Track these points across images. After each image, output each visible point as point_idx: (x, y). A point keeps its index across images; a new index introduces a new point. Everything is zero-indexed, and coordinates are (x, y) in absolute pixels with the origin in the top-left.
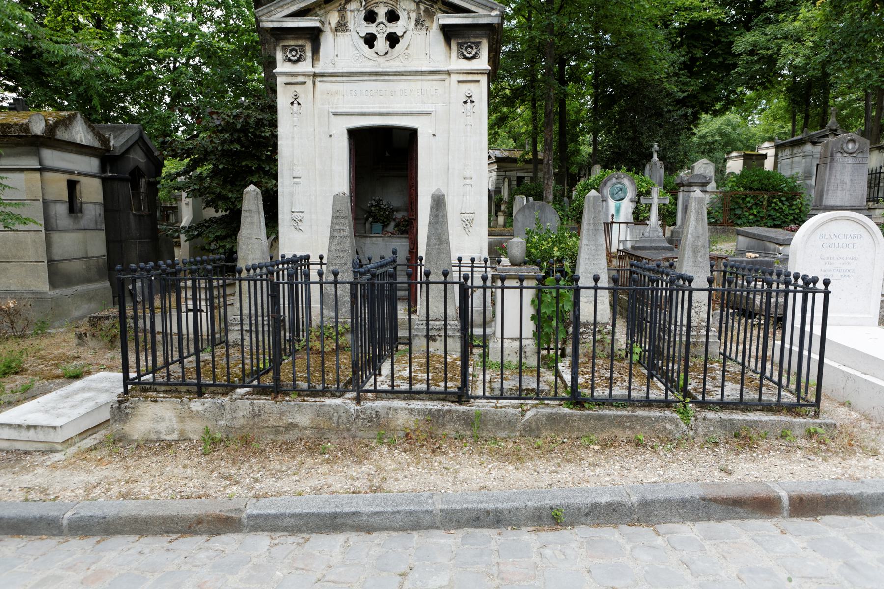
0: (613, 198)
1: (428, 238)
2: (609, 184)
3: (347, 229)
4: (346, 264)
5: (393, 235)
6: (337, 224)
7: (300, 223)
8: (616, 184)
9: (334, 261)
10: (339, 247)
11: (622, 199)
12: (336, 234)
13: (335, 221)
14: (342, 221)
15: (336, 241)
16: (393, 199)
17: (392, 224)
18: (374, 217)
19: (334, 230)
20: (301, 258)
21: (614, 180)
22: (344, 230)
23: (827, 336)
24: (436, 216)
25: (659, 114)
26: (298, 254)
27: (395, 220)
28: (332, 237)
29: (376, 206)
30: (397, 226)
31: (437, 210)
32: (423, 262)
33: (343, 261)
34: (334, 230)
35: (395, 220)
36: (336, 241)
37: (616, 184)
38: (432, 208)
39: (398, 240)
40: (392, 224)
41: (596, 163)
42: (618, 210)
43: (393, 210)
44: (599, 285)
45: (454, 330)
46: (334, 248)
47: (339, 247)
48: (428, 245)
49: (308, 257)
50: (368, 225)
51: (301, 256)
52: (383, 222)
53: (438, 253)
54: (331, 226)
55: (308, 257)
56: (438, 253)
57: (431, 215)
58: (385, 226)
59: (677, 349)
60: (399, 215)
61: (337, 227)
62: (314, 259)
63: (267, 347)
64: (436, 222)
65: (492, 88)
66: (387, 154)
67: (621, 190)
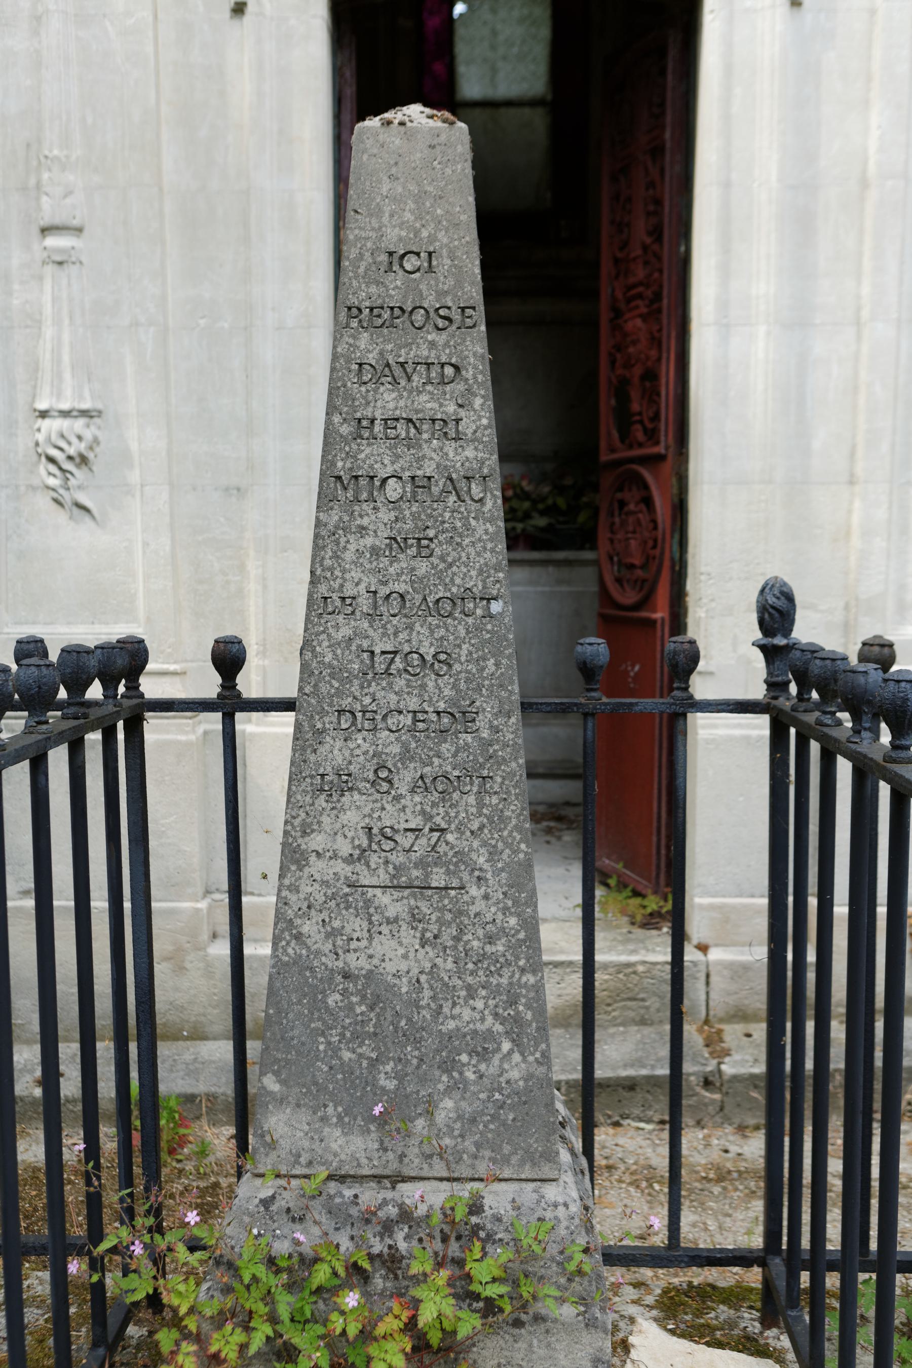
3: (480, 417)
4: (465, 717)
6: (390, 372)
7: (80, 475)
9: (358, 696)
10: (401, 573)
12: (376, 457)
13: (368, 347)
14: (429, 345)
15: (378, 521)
19: (363, 427)
20: (78, 666)
22: (446, 428)
23: (577, 930)
26: (58, 636)
28: (342, 486)
33: (440, 691)
34: (363, 427)
36: (378, 521)
46: (358, 582)
47: (401, 573)
49: (127, 660)
51: (72, 652)
54: (336, 395)
55: (127, 660)
59: (838, 1031)
61: (388, 401)
62: (177, 670)
63: (63, 899)
65: (683, 249)
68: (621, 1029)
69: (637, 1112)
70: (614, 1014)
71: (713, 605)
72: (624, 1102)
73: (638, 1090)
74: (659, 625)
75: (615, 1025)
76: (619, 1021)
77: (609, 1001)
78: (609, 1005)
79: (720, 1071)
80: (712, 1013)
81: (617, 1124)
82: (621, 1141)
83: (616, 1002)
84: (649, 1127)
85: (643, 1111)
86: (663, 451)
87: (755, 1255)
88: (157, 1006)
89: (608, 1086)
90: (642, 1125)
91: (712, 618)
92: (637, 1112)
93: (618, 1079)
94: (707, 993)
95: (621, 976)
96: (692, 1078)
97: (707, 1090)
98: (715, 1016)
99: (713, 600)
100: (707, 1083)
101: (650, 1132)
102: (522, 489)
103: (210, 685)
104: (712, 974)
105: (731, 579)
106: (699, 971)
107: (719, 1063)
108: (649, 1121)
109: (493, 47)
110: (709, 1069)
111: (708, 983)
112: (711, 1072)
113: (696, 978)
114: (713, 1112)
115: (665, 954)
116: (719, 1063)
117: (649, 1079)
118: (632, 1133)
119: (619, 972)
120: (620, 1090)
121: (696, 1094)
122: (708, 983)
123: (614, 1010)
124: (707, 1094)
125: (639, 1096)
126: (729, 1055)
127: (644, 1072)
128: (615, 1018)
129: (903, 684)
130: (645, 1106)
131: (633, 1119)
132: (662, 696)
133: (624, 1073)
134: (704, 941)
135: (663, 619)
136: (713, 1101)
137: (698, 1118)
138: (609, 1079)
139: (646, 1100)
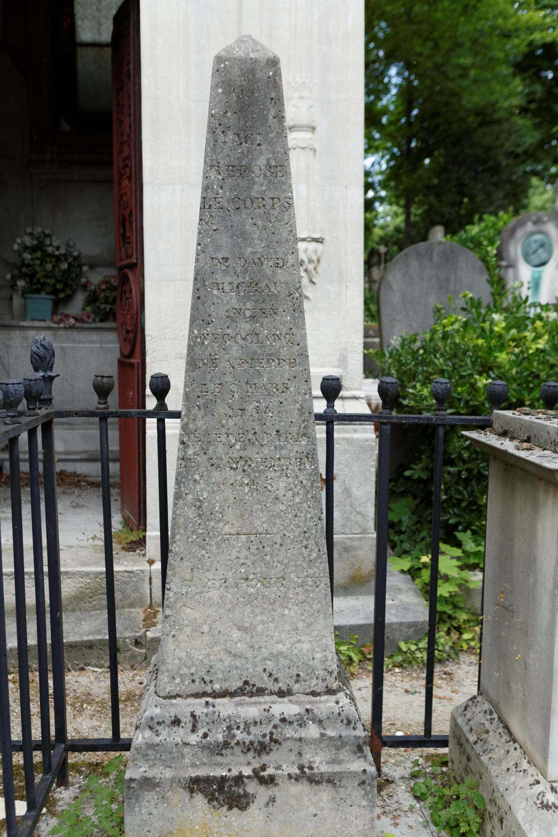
0: (528, 261)
1: (201, 281)
2: (520, 233)
5: (80, 324)
8: (532, 234)
11: (543, 264)
16: (83, 237)
17: (80, 299)
18: (31, 277)
21: (530, 227)
24: (240, 170)
25: (496, 170)
27: (85, 287)
29: (33, 249)
30: (92, 300)
31: (244, 136)
32: (174, 401)
35: (85, 287)
37: (532, 234)
38: (216, 128)
39: (94, 336)
40: (80, 299)
41: (433, 224)
42: (536, 285)
43: (77, 263)
44: (340, 407)
45: (339, 743)
48: (199, 317)
50: (17, 301)
52: (55, 292)
53: (253, 358)
56: (253, 358)
57: (211, 164)
58: (59, 302)
60: (95, 278)
64: (239, 203)
66: (66, 127)
67: (542, 245)
68: (98, 612)
69: (94, 661)
70: (94, 603)
71: (155, 354)
72: (86, 655)
73: (95, 648)
74: (136, 365)
75: (94, 610)
76: (97, 607)
77: (91, 595)
78: (91, 597)
79: (145, 636)
80: (153, 601)
81: (82, 669)
82: (80, 679)
83: (95, 595)
84: (99, 670)
85: (98, 661)
86: (135, 261)
87: (106, 742)
88: (35, 616)
89: (76, 646)
90: (96, 669)
91: (154, 362)
92: (94, 661)
93: (82, 642)
94: (151, 589)
95: (98, 580)
96: (127, 640)
97: (137, 647)
98: (155, 603)
99: (154, 352)
100: (137, 643)
101: (100, 674)
102: (111, 284)
103: (91, 401)
104: (153, 577)
105: (165, 338)
106: (145, 576)
107: (146, 631)
108: (100, 667)
109: (98, 10)
110: (138, 634)
111: (151, 583)
112: (139, 636)
113: (143, 580)
114: (140, 661)
115: (102, 566)
116: (146, 631)
117: (100, 641)
118: (90, 674)
119: (97, 578)
120: (84, 648)
121: (130, 650)
122: (151, 583)
123: (94, 601)
124: (137, 650)
125: (95, 652)
126: (155, 626)
127: (99, 637)
128: (95, 605)
129: (9, 386)
130: (99, 658)
131: (92, 666)
132: (138, 408)
133: (86, 638)
134: (152, 558)
135: (138, 363)
136: (140, 654)
137: (132, 664)
138: (77, 642)
139: (100, 654)
